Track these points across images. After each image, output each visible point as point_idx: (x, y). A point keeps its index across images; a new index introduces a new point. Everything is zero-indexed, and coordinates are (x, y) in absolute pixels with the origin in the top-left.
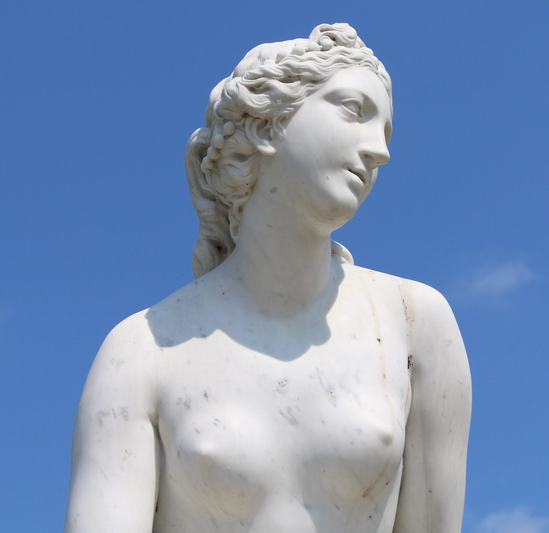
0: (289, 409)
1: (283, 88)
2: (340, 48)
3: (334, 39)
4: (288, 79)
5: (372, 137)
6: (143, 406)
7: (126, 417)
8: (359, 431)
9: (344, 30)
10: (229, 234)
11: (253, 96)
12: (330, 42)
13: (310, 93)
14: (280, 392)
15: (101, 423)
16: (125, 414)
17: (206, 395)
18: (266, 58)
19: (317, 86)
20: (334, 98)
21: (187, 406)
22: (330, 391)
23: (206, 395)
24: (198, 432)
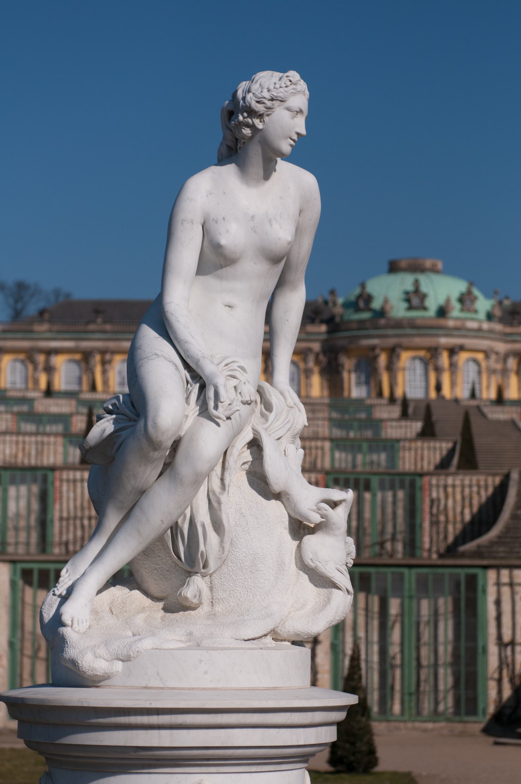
0: (254, 227)
1: (269, 104)
2: (293, 86)
3: (290, 81)
4: (272, 100)
5: (299, 125)
6: (199, 220)
7: (193, 223)
8: (280, 239)
9: (294, 75)
10: (237, 143)
11: (257, 104)
12: (289, 83)
13: (279, 106)
14: (252, 220)
15: (182, 223)
16: (192, 222)
17: (224, 219)
18: (329, 298)
19: (282, 103)
20: (288, 109)
21: (216, 222)
22: (270, 221)
23: (224, 219)
24: (220, 234)
